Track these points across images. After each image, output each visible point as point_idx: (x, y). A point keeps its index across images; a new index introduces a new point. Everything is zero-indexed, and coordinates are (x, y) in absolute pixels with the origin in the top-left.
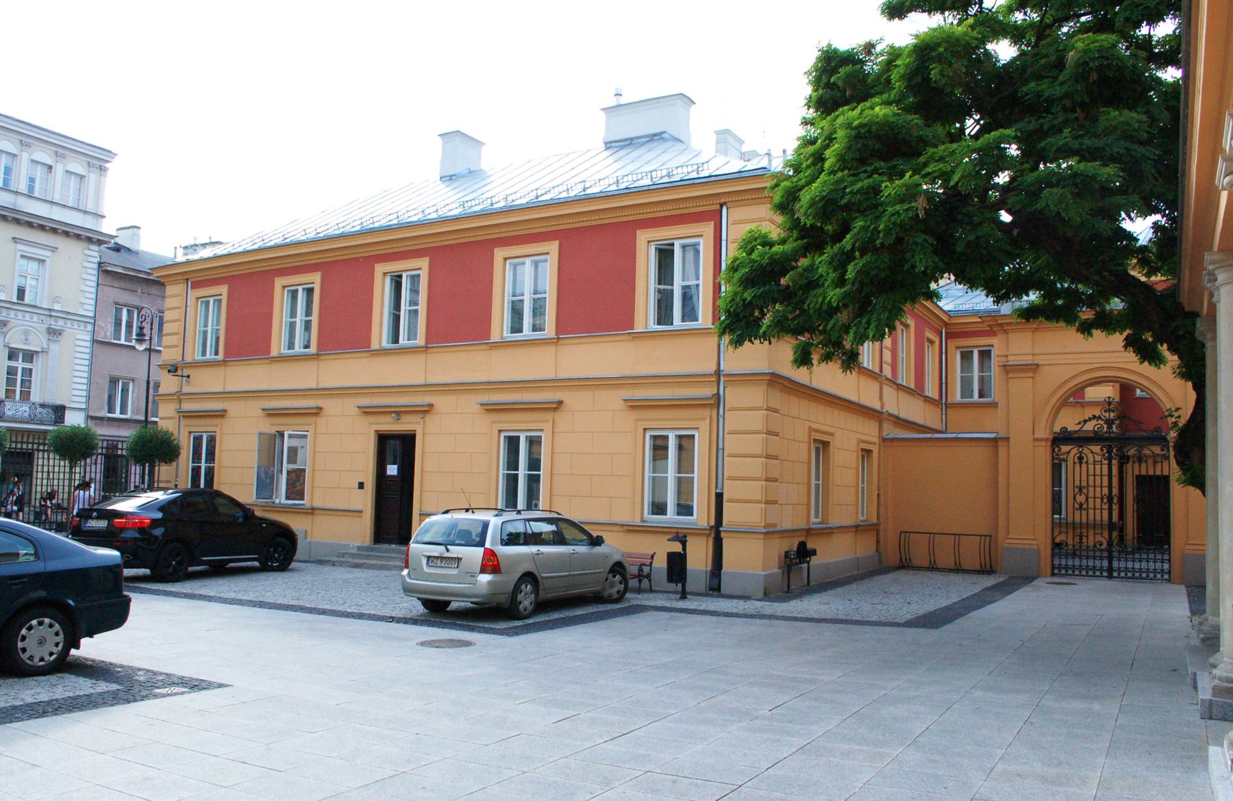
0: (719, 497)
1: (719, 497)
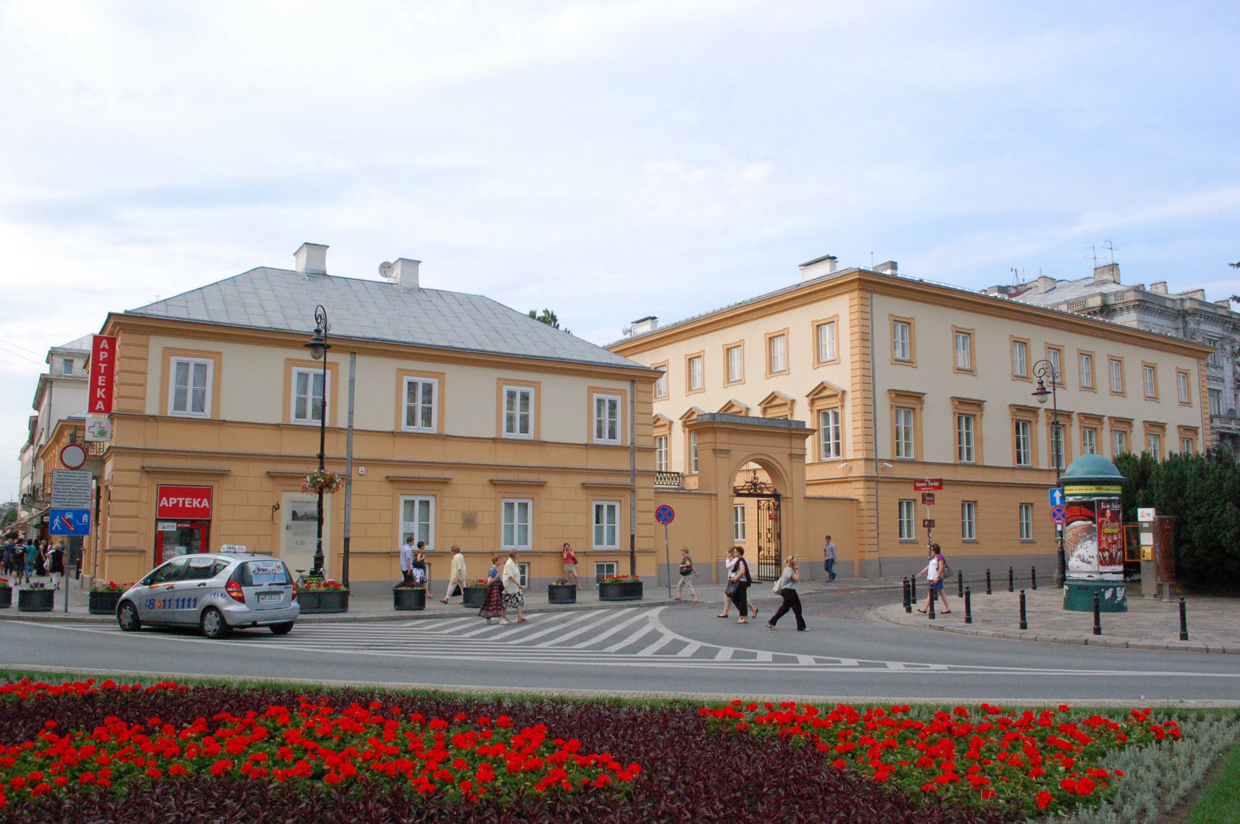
1: (632, 537)
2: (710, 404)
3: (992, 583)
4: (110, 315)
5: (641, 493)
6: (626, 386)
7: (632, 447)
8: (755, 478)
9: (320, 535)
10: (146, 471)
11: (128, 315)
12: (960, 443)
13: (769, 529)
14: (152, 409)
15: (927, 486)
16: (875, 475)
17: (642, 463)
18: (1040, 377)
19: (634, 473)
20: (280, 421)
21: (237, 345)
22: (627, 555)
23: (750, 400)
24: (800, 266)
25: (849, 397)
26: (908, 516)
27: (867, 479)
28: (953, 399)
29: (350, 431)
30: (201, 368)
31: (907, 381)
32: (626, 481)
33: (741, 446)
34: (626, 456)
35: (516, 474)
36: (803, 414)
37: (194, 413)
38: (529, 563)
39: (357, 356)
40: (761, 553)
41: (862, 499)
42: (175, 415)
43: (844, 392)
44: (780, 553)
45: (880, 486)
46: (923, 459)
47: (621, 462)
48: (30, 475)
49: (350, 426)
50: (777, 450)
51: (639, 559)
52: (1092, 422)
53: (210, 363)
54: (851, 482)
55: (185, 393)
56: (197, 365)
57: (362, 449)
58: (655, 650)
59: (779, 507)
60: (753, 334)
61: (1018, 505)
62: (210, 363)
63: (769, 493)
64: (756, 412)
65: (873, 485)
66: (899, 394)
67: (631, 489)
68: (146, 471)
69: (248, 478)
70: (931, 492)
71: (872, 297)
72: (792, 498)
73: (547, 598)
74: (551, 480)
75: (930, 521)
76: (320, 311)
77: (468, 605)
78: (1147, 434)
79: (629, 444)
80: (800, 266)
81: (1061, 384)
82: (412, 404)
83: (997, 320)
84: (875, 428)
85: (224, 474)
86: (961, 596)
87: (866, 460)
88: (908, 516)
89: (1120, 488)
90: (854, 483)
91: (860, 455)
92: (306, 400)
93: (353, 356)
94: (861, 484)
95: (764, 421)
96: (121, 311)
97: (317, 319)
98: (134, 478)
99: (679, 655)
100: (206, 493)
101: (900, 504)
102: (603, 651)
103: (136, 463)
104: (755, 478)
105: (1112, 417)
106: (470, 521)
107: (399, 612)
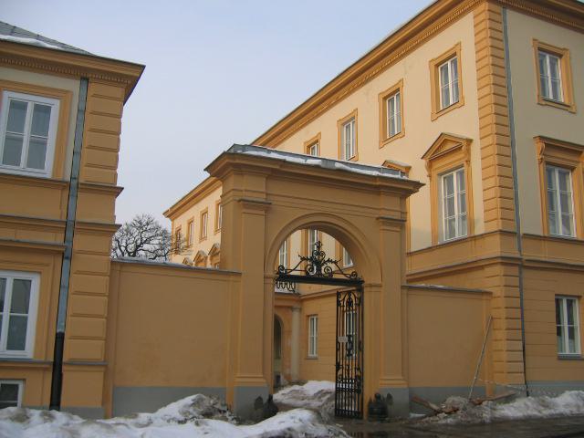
0: (60, 338)
1: (60, 338)
5: (79, 263)
6: (73, 86)
7: (74, 182)
8: (318, 253)
12: (463, 196)
16: (518, 256)
17: (86, 210)
19: (68, 226)
21: (47, 76)
22: (45, 369)
25: (476, 150)
26: (571, 321)
27: (507, 261)
30: (43, 111)
32: (54, 238)
33: (293, 199)
34: (57, 196)
35: (18, 238)
37: (30, 169)
38: (24, 380)
40: (340, 372)
41: (498, 291)
43: (470, 141)
44: (362, 373)
45: (526, 273)
47: (49, 206)
50: (357, 212)
51: (68, 377)
53: (55, 105)
54: (482, 267)
56: (38, 108)
59: (361, 301)
61: (553, 298)
62: (55, 105)
63: (342, 277)
65: (515, 270)
66: (551, 145)
67: (65, 254)
71: (505, 13)
72: (265, 277)
78: (549, 165)
79: (68, 178)
82: (15, 134)
83: (534, 19)
84: (516, 188)
87: (502, 232)
88: (571, 321)
90: (487, 269)
91: (495, 226)
93: (85, 82)
94: (499, 270)
101: (558, 302)
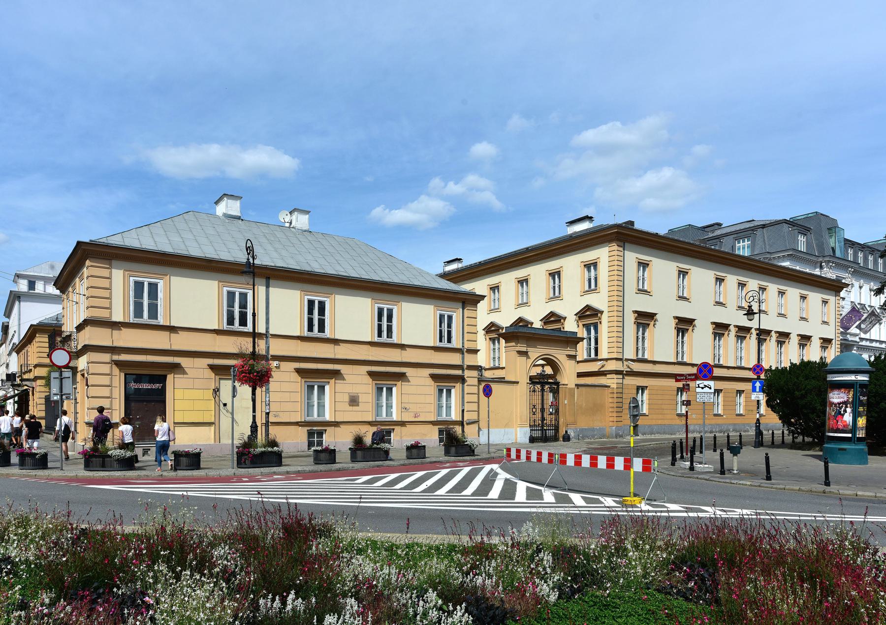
2: (505, 320)
3: (781, 436)
4: (79, 243)
8: (543, 371)
9: (254, 411)
10: (118, 364)
11: (92, 244)
13: (534, 406)
14: (118, 317)
15: (686, 379)
18: (750, 302)
20: (217, 328)
23: (535, 317)
24: (566, 223)
28: (676, 318)
29: (266, 336)
31: (646, 307)
36: (571, 325)
39: (271, 282)
42: (135, 322)
46: (653, 359)
47: (455, 359)
48: (5, 365)
49: (267, 331)
52: (783, 337)
55: (142, 304)
57: (277, 348)
58: (447, 490)
60: (538, 272)
64: (538, 324)
68: (118, 364)
69: (197, 368)
70: (688, 383)
71: (624, 245)
73: (83, 467)
74: (408, 371)
75: (687, 401)
76: (249, 244)
77: (88, 469)
80: (566, 223)
81: (765, 312)
85: (176, 368)
86: (715, 451)
89: (868, 375)
92: (233, 312)
95: (542, 331)
96: (87, 240)
97: (247, 250)
98: (106, 369)
99: (463, 493)
100: (162, 379)
102: (435, 494)
103: (106, 357)
104: (543, 371)
105: (800, 335)
106: (354, 401)
107: (317, 466)
